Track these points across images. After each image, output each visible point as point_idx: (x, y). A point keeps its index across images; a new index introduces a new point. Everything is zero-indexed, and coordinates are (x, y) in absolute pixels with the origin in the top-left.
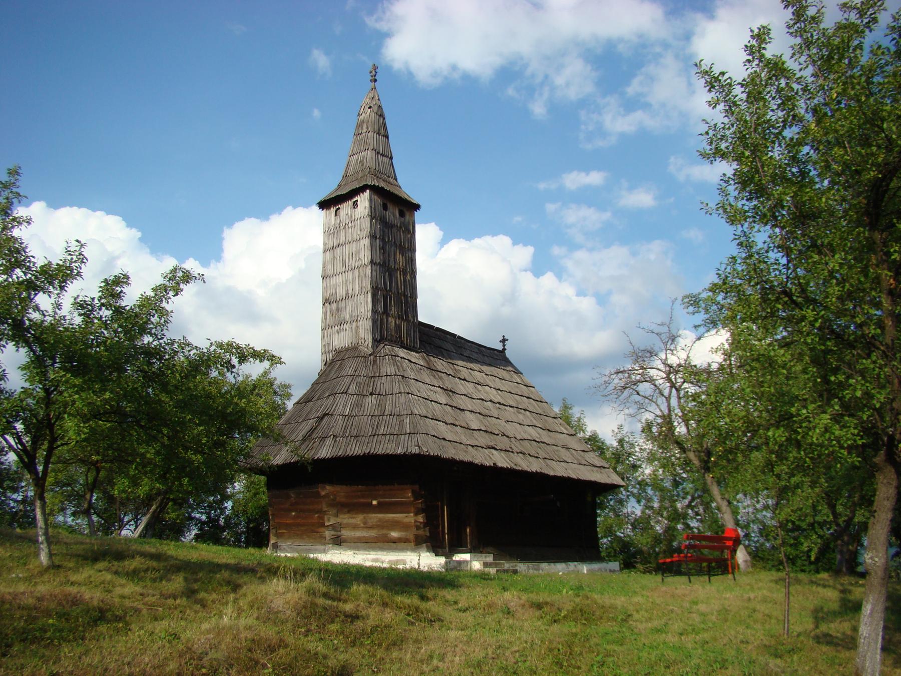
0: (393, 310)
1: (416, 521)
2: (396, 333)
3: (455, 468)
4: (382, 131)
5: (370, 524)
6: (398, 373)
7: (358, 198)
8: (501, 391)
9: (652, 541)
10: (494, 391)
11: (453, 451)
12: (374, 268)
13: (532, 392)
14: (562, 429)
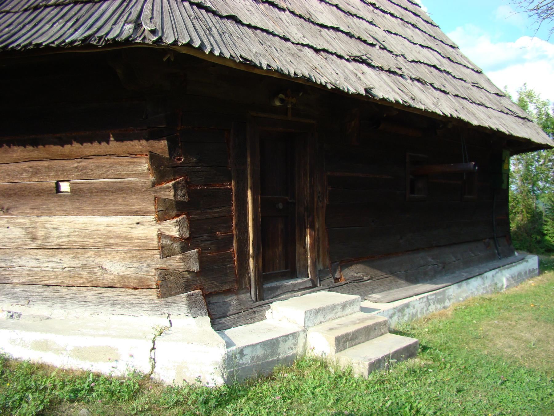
1: (161, 236)
3: (278, 103)
14: (465, 62)
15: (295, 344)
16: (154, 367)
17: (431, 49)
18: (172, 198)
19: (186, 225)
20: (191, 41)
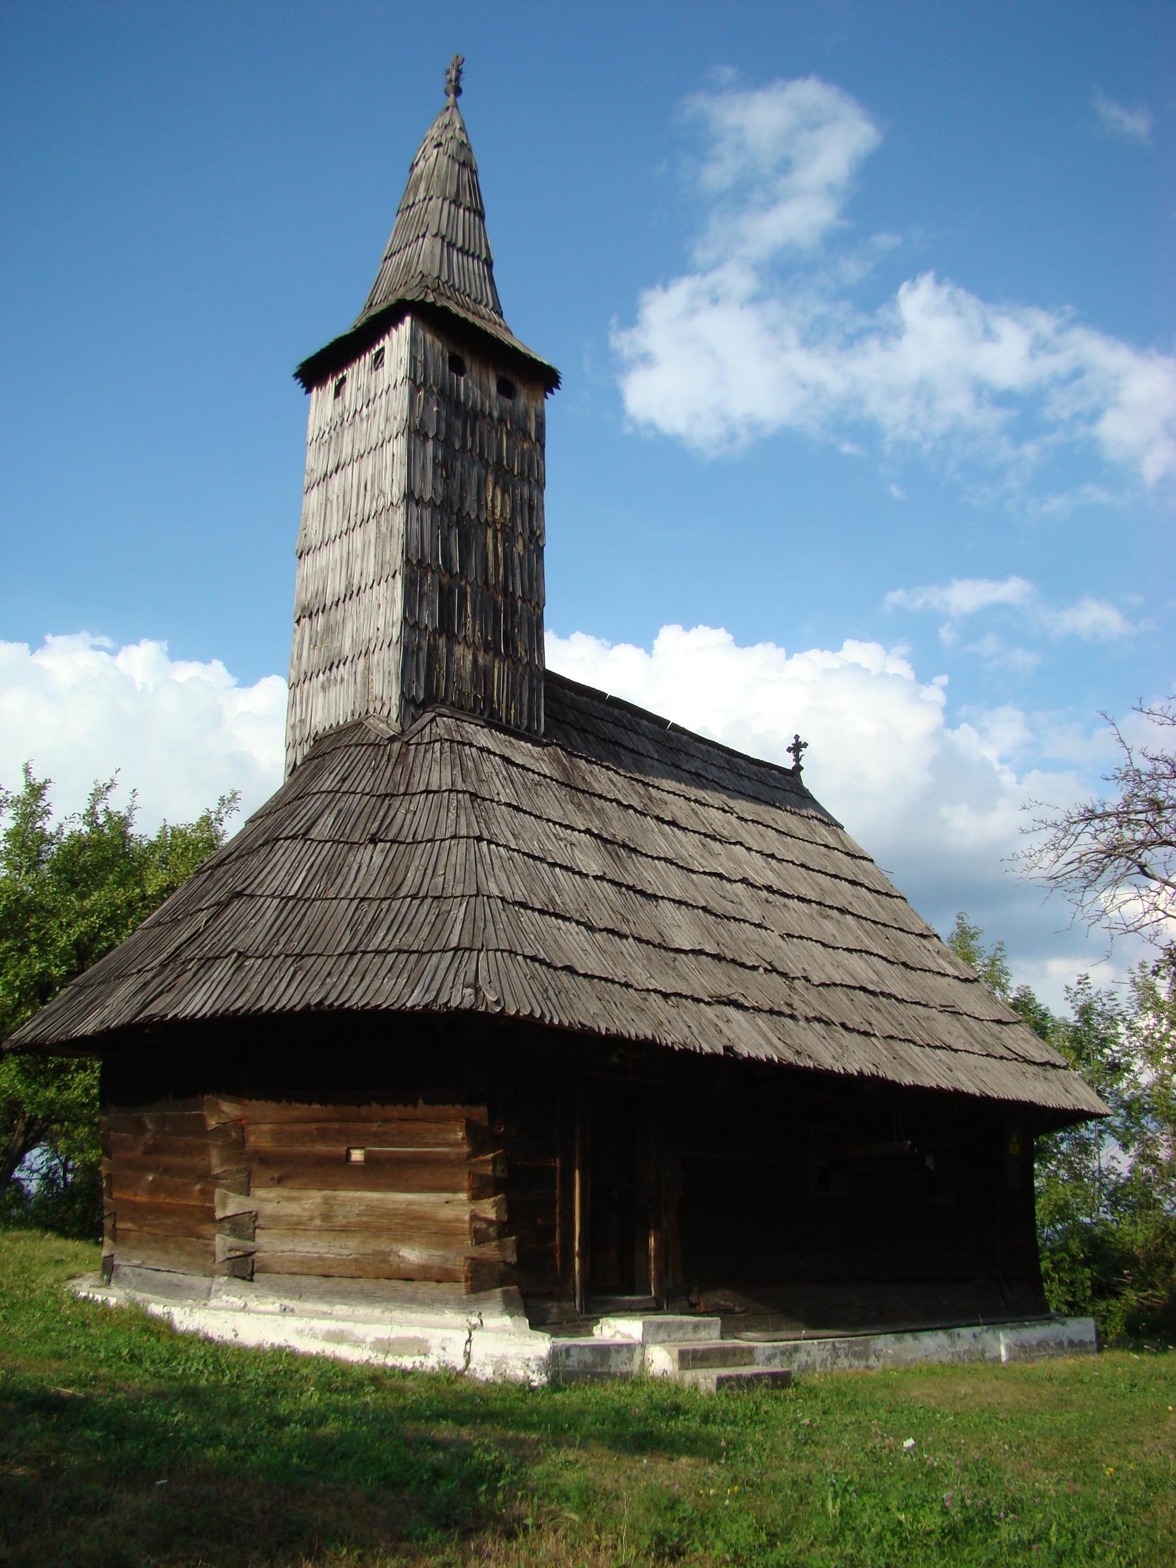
0: (470, 628)
1: (474, 1217)
2: (476, 686)
3: (615, 1059)
4: (467, 200)
5: (340, 1220)
6: (460, 785)
7: (385, 343)
8: (780, 860)
9: (1156, 1237)
10: (759, 860)
11: (594, 1007)
12: (415, 511)
13: (865, 871)
15: (631, 1359)
16: (468, 1362)
17: (867, 952)
18: (490, 1173)
19: (504, 1206)
20: (532, 1011)
